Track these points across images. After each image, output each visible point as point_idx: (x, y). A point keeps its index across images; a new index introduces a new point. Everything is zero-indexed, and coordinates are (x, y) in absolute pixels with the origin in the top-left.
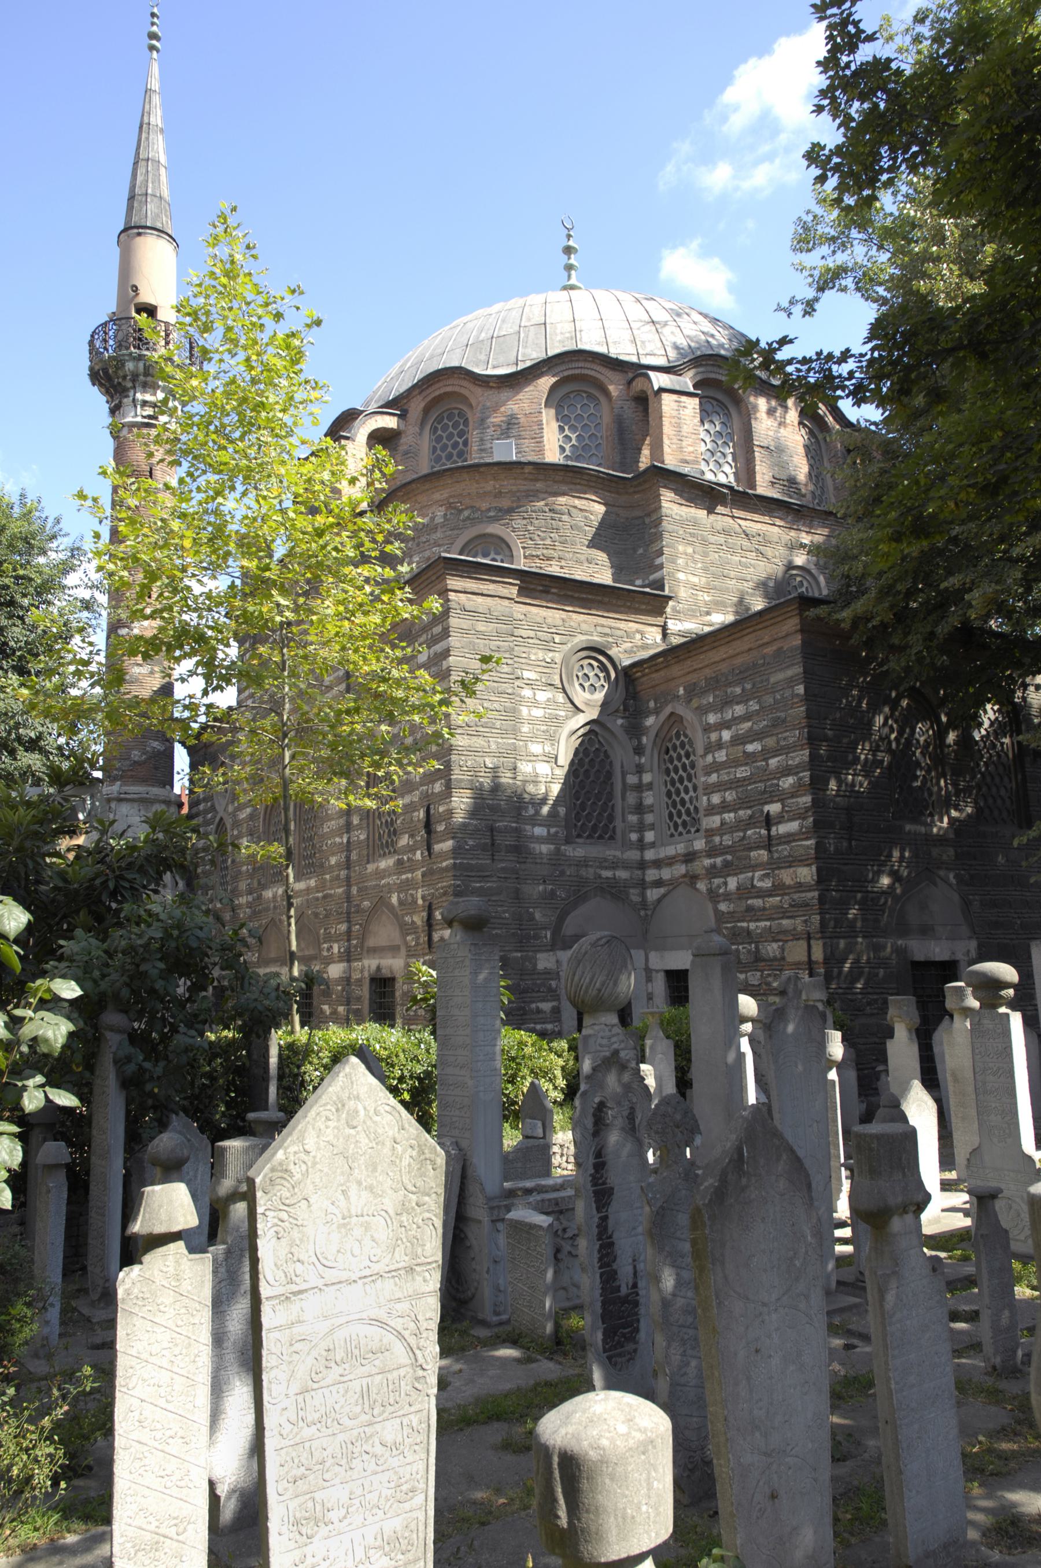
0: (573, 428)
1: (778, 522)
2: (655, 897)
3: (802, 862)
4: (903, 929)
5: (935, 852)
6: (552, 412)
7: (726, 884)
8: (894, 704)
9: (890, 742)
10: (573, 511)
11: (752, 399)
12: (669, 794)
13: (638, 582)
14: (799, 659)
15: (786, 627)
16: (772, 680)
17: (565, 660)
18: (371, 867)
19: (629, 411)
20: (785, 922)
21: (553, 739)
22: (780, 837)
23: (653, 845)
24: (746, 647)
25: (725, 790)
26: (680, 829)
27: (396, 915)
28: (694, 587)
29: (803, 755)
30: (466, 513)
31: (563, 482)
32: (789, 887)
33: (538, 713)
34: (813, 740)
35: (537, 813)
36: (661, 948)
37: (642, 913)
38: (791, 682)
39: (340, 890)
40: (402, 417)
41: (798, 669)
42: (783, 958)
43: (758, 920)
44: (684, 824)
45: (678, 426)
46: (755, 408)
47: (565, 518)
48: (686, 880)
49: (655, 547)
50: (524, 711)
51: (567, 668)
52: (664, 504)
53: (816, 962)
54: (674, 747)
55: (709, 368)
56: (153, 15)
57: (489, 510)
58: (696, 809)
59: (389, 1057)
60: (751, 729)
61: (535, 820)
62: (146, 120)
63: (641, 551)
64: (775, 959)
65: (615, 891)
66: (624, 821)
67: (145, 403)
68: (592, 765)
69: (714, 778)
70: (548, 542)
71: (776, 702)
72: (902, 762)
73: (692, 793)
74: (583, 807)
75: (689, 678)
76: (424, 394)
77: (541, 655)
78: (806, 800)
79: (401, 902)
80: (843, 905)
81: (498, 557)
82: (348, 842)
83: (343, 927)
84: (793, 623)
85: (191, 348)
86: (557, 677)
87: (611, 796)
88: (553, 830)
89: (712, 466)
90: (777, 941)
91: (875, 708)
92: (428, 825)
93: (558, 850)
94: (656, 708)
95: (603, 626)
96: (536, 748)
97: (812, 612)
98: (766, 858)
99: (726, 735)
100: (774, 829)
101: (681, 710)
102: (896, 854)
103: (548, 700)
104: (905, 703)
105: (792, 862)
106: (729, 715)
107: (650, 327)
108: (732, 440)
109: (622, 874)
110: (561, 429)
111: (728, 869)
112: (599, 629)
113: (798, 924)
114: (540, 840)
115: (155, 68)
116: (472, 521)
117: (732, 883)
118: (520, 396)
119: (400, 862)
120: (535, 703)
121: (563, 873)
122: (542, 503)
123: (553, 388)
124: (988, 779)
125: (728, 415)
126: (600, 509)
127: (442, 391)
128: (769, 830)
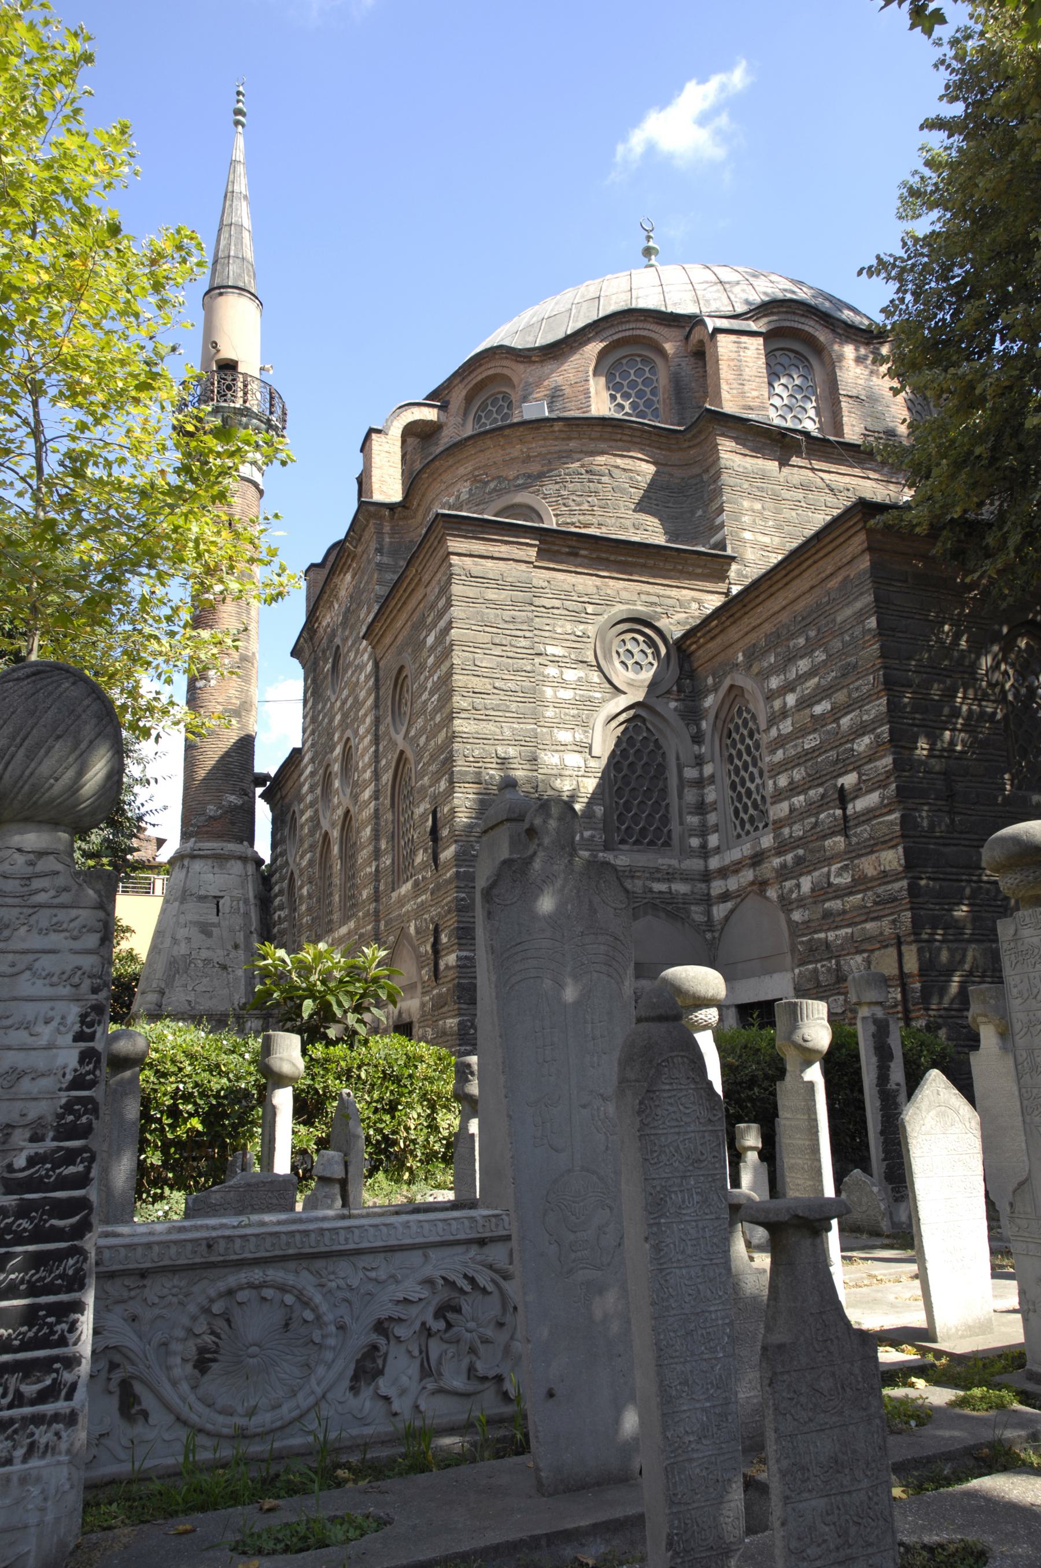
0: (626, 396)
1: (872, 475)
2: (722, 915)
3: (887, 844)
6: (602, 380)
7: (798, 886)
8: (1008, 645)
9: (1004, 692)
10: (616, 472)
11: (836, 347)
14: (868, 585)
15: (850, 549)
16: (839, 619)
17: (601, 634)
18: (394, 895)
19: (687, 367)
21: (585, 725)
22: (858, 815)
23: (718, 850)
24: (807, 586)
25: (793, 767)
26: (747, 826)
29: (881, 704)
30: (492, 485)
31: (601, 439)
32: (873, 879)
33: (567, 694)
34: (891, 685)
37: (709, 936)
38: (860, 616)
39: (369, 927)
40: (443, 408)
41: (869, 598)
43: (837, 928)
44: (752, 819)
45: (739, 371)
46: (841, 357)
47: (604, 479)
48: (755, 888)
49: (715, 506)
50: (549, 692)
51: (603, 641)
52: (722, 454)
53: (910, 975)
54: (736, 728)
55: (783, 316)
56: (239, 93)
57: (517, 478)
58: (763, 797)
59: (161, 1061)
62: (230, 189)
63: (700, 513)
66: (681, 823)
68: (637, 758)
69: (780, 755)
70: (586, 506)
71: (845, 645)
73: (758, 781)
74: (627, 807)
75: (747, 640)
76: (466, 381)
77: (569, 627)
78: (887, 762)
82: (377, 870)
84: (859, 541)
85: (272, 398)
87: (664, 791)
90: (859, 952)
91: (979, 647)
92: (434, 832)
94: (715, 684)
95: (649, 594)
96: (564, 736)
97: (877, 521)
98: (842, 846)
99: (791, 699)
100: (850, 806)
101: (740, 679)
103: (579, 679)
104: (1023, 643)
105: (873, 847)
106: (792, 675)
107: (719, 287)
108: (815, 393)
109: (680, 888)
110: (613, 398)
111: (801, 867)
112: (644, 597)
113: (883, 926)
115: (240, 142)
116: (498, 492)
117: (806, 884)
118: (565, 367)
119: (416, 884)
120: (563, 684)
122: (578, 464)
123: (602, 355)
125: (809, 367)
126: (648, 469)
127: (484, 375)
128: (844, 809)
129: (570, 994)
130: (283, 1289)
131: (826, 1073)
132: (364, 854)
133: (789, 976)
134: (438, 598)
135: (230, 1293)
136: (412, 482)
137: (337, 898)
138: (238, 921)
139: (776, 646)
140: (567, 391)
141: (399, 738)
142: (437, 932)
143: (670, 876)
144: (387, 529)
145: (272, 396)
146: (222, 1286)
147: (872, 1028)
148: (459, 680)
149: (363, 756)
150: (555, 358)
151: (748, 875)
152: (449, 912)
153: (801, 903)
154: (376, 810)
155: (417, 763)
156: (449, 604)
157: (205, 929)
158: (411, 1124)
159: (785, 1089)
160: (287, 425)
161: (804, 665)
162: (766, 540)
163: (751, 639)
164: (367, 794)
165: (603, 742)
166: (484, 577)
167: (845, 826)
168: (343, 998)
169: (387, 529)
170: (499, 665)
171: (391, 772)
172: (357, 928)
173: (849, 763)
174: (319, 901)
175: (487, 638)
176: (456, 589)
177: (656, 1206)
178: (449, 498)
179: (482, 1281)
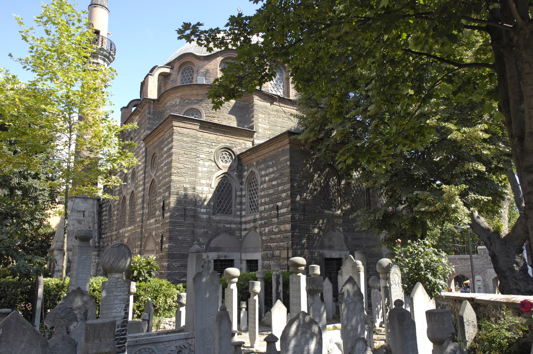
1: (296, 108)
4: (322, 247)
5: (335, 220)
9: (321, 183)
12: (250, 199)
13: (246, 126)
17: (216, 152)
18: (148, 222)
20: (281, 243)
21: (210, 178)
22: (281, 214)
23: (244, 216)
27: (154, 239)
28: (264, 129)
29: (288, 186)
30: (187, 101)
32: (283, 231)
33: (205, 169)
34: (292, 180)
35: (203, 204)
36: (245, 252)
37: (240, 240)
38: (286, 161)
40: (172, 68)
41: (288, 156)
42: (280, 256)
43: (274, 243)
50: (200, 169)
51: (217, 154)
54: (252, 182)
60: (274, 177)
61: (201, 206)
64: (278, 256)
65: (231, 232)
67: (93, 63)
68: (224, 189)
71: (282, 167)
72: (326, 188)
74: (220, 202)
75: (257, 159)
77: (207, 149)
79: (156, 235)
80: (301, 238)
81: (197, 116)
83: (139, 243)
84: (287, 141)
85: (111, 45)
86: (213, 158)
88: (208, 210)
89: (275, 89)
91: (315, 171)
92: (163, 207)
93: (210, 217)
96: (203, 182)
97: (293, 137)
99: (267, 178)
102: (321, 221)
105: (284, 223)
109: (233, 226)
114: (203, 213)
117: (267, 229)
118: (211, 63)
119: (156, 220)
120: (204, 166)
121: (211, 225)
124: (357, 196)
125: (282, 72)
129: (207, 296)
130: (149, 349)
131: (259, 297)
132: (139, 207)
133: (260, 254)
134: (169, 138)
135: (140, 350)
136: (161, 95)
137: (127, 218)
138: (91, 219)
139: (264, 163)
140: (211, 71)
141: (153, 175)
142: (162, 237)
143: (231, 223)
144: (152, 107)
145: (111, 44)
146: (138, 349)
147: (276, 277)
148: (174, 164)
149: (140, 176)
150: (208, 60)
151: (252, 225)
152: (167, 232)
153: (265, 234)
154: (144, 195)
155: (159, 184)
156: (172, 141)
157: (79, 222)
158: (160, 302)
159: (250, 300)
160: (116, 54)
161: (271, 170)
162: (265, 126)
163: (258, 159)
164: (141, 189)
165: (215, 184)
166: (183, 134)
167: (278, 216)
168: (144, 270)
169: (152, 107)
170: (186, 160)
171: (149, 184)
172: (134, 229)
173: (279, 199)
174: (120, 217)
175: (183, 152)
176: (175, 137)
177: (220, 339)
178: (174, 100)
179: (186, 346)
